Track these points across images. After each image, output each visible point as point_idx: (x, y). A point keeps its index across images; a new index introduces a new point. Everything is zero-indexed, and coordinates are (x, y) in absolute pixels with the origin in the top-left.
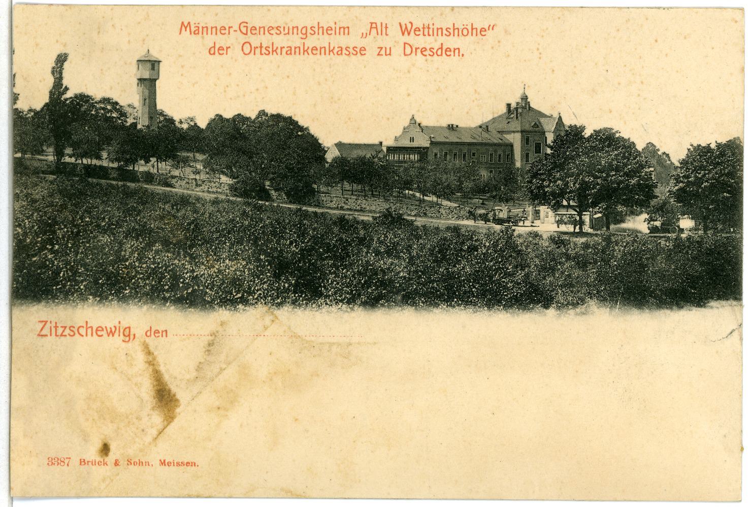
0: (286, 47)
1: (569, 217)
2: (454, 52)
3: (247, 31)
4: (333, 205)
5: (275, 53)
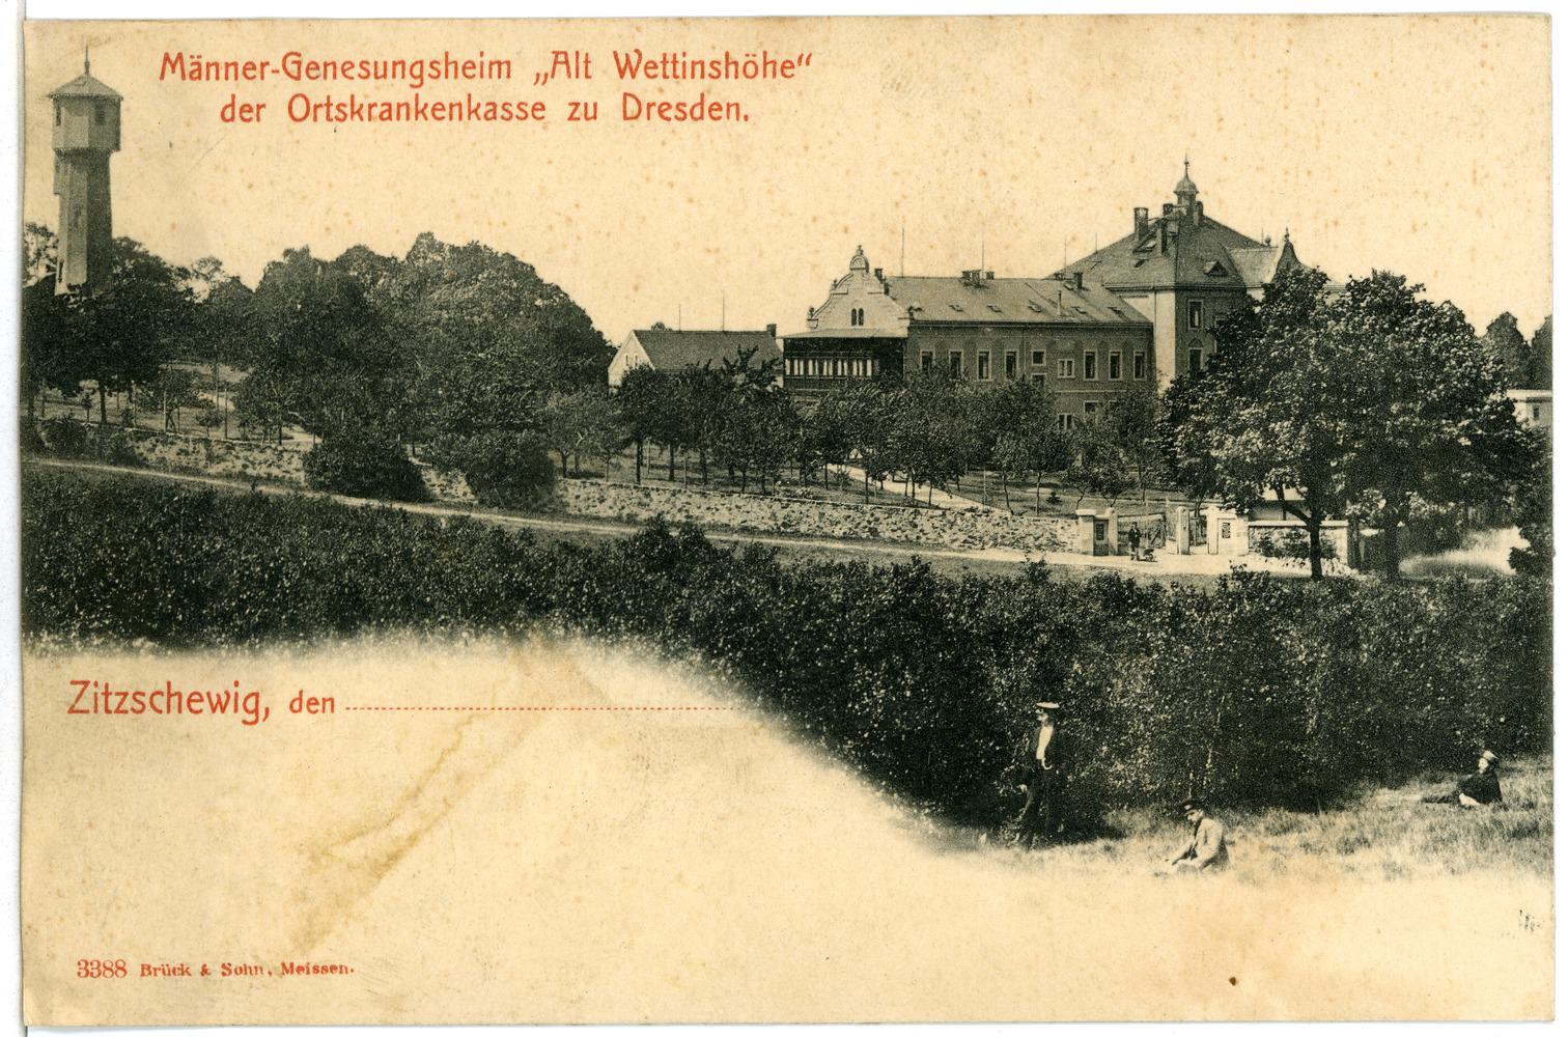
0: (379, 104)
1: (1288, 536)
2: (728, 110)
4: (604, 510)
5: (356, 117)
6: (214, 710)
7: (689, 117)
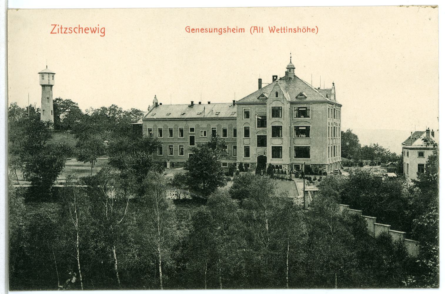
3: (189, 31)
6: (92, 32)
7: (73, 32)
